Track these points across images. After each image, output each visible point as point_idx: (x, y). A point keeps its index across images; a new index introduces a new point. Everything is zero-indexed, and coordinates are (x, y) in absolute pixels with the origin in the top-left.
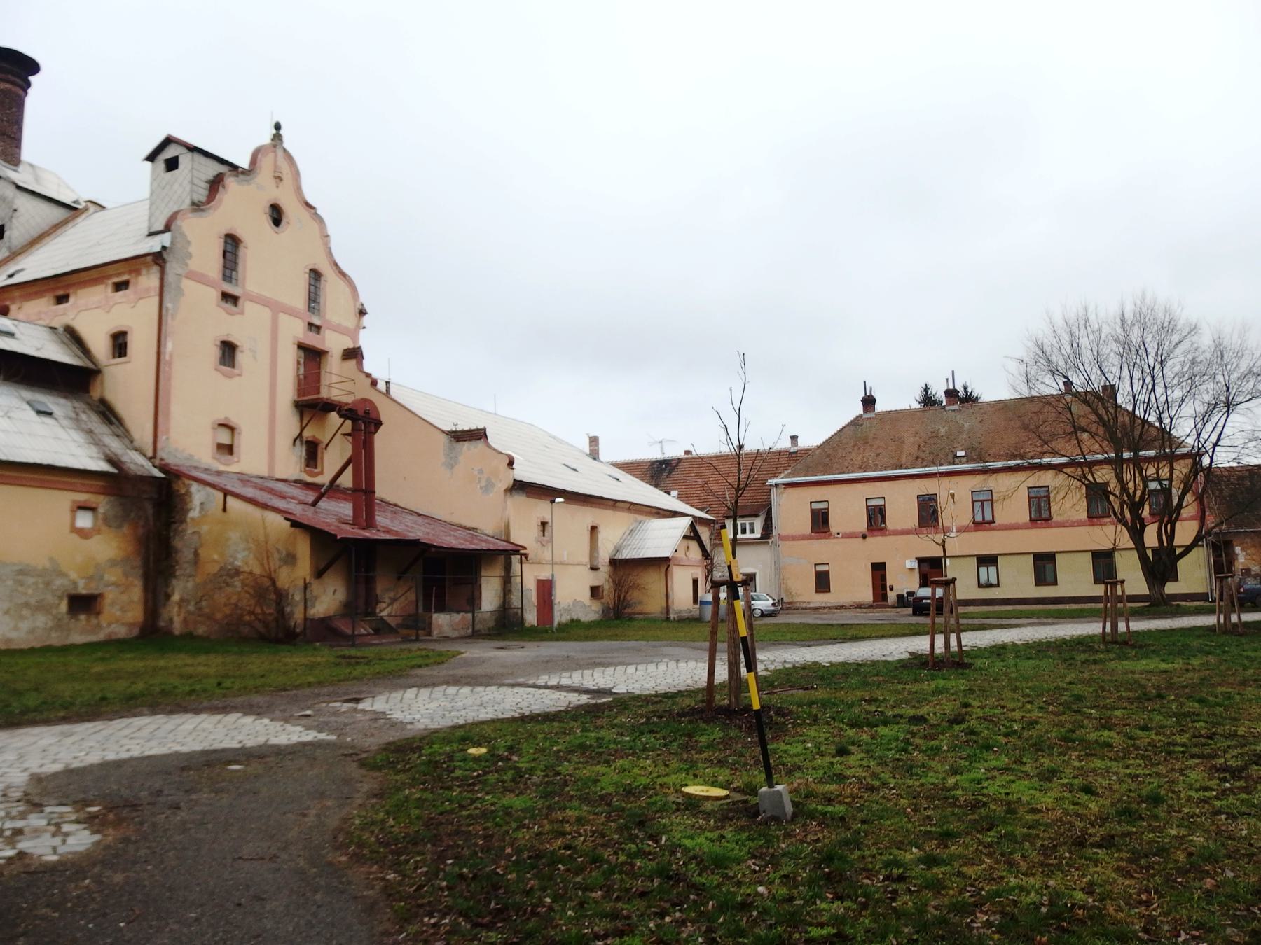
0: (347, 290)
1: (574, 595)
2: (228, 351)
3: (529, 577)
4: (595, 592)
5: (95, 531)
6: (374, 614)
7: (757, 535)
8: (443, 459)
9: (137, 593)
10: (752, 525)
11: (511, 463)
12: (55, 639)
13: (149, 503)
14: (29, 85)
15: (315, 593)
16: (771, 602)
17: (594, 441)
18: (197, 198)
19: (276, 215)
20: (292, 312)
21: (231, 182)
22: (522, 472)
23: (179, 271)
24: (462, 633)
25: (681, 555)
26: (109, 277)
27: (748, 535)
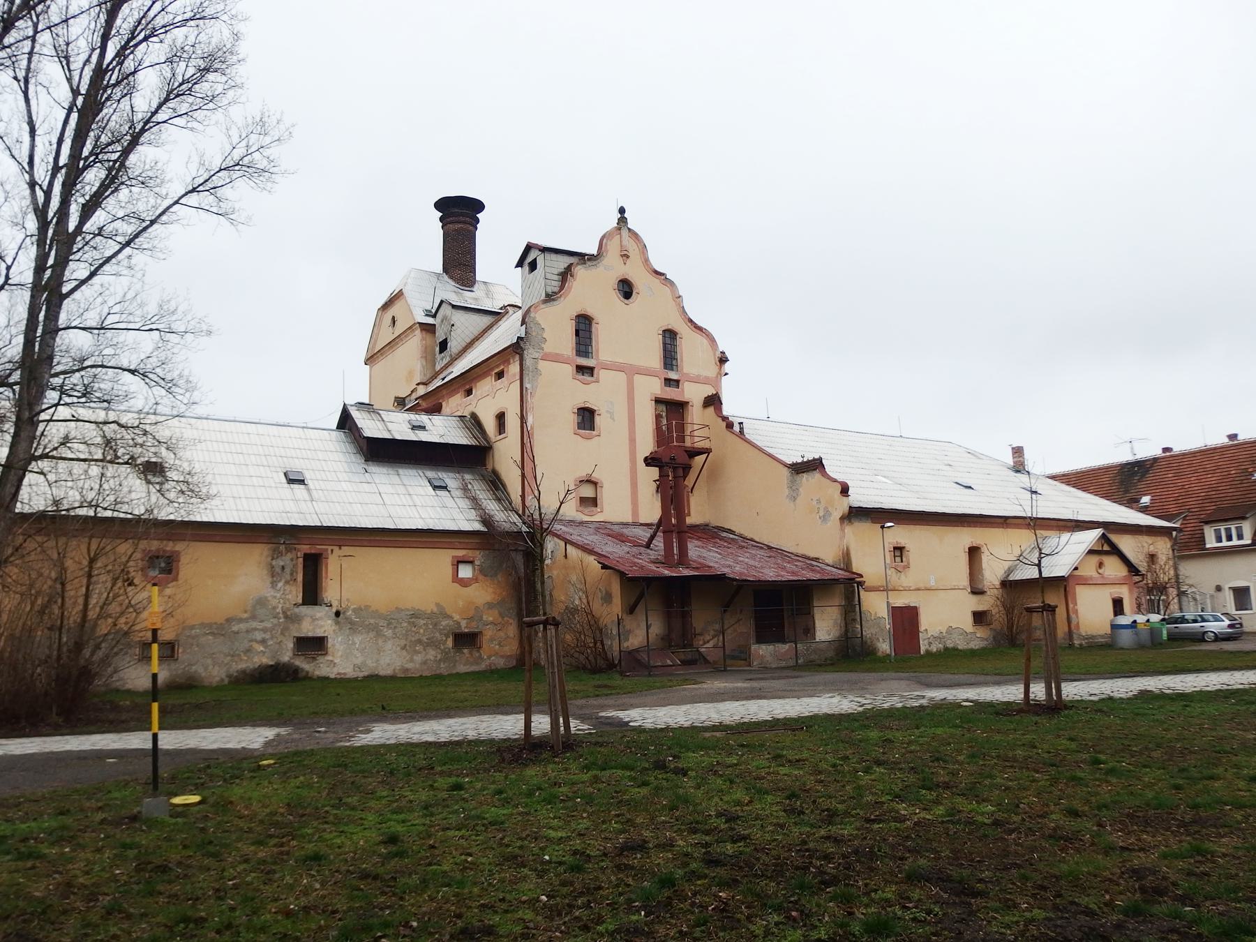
0: (705, 341)
1: (947, 616)
2: (586, 417)
3: (876, 606)
4: (979, 617)
5: (474, 580)
6: (691, 646)
7: (1247, 540)
8: (787, 492)
9: (512, 630)
10: (1239, 530)
11: (845, 490)
12: (444, 669)
13: (512, 551)
14: (478, 221)
15: (628, 627)
16: (1227, 622)
17: (1018, 451)
18: (549, 290)
19: (626, 289)
20: (648, 373)
21: (580, 271)
22: (861, 496)
23: (536, 355)
24: (783, 664)
25: (1089, 570)
26: (492, 369)
27: (1235, 542)
